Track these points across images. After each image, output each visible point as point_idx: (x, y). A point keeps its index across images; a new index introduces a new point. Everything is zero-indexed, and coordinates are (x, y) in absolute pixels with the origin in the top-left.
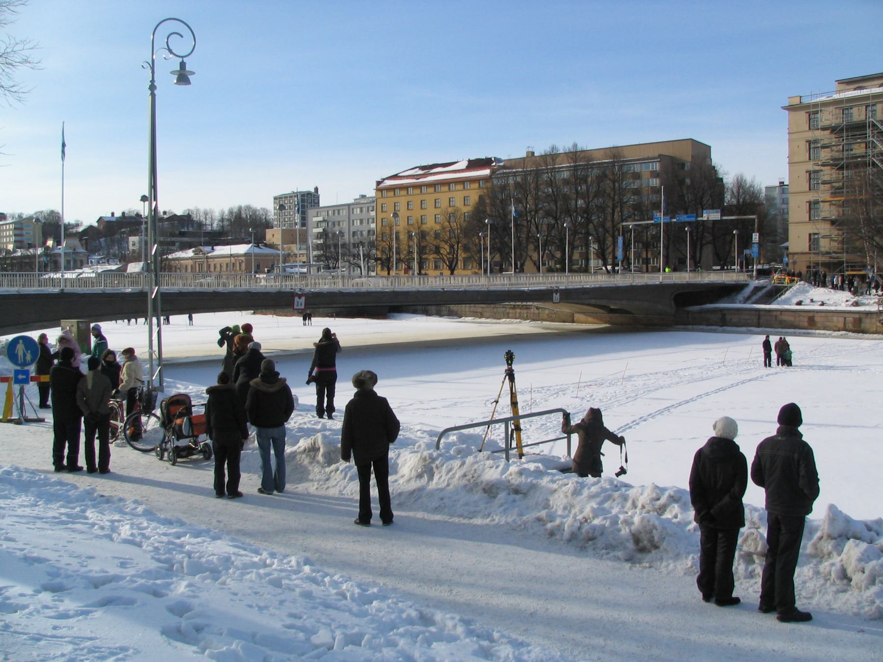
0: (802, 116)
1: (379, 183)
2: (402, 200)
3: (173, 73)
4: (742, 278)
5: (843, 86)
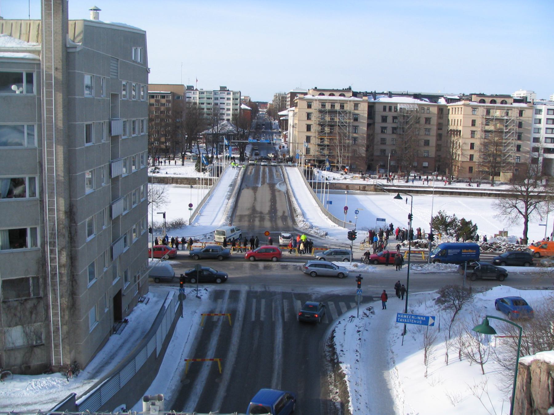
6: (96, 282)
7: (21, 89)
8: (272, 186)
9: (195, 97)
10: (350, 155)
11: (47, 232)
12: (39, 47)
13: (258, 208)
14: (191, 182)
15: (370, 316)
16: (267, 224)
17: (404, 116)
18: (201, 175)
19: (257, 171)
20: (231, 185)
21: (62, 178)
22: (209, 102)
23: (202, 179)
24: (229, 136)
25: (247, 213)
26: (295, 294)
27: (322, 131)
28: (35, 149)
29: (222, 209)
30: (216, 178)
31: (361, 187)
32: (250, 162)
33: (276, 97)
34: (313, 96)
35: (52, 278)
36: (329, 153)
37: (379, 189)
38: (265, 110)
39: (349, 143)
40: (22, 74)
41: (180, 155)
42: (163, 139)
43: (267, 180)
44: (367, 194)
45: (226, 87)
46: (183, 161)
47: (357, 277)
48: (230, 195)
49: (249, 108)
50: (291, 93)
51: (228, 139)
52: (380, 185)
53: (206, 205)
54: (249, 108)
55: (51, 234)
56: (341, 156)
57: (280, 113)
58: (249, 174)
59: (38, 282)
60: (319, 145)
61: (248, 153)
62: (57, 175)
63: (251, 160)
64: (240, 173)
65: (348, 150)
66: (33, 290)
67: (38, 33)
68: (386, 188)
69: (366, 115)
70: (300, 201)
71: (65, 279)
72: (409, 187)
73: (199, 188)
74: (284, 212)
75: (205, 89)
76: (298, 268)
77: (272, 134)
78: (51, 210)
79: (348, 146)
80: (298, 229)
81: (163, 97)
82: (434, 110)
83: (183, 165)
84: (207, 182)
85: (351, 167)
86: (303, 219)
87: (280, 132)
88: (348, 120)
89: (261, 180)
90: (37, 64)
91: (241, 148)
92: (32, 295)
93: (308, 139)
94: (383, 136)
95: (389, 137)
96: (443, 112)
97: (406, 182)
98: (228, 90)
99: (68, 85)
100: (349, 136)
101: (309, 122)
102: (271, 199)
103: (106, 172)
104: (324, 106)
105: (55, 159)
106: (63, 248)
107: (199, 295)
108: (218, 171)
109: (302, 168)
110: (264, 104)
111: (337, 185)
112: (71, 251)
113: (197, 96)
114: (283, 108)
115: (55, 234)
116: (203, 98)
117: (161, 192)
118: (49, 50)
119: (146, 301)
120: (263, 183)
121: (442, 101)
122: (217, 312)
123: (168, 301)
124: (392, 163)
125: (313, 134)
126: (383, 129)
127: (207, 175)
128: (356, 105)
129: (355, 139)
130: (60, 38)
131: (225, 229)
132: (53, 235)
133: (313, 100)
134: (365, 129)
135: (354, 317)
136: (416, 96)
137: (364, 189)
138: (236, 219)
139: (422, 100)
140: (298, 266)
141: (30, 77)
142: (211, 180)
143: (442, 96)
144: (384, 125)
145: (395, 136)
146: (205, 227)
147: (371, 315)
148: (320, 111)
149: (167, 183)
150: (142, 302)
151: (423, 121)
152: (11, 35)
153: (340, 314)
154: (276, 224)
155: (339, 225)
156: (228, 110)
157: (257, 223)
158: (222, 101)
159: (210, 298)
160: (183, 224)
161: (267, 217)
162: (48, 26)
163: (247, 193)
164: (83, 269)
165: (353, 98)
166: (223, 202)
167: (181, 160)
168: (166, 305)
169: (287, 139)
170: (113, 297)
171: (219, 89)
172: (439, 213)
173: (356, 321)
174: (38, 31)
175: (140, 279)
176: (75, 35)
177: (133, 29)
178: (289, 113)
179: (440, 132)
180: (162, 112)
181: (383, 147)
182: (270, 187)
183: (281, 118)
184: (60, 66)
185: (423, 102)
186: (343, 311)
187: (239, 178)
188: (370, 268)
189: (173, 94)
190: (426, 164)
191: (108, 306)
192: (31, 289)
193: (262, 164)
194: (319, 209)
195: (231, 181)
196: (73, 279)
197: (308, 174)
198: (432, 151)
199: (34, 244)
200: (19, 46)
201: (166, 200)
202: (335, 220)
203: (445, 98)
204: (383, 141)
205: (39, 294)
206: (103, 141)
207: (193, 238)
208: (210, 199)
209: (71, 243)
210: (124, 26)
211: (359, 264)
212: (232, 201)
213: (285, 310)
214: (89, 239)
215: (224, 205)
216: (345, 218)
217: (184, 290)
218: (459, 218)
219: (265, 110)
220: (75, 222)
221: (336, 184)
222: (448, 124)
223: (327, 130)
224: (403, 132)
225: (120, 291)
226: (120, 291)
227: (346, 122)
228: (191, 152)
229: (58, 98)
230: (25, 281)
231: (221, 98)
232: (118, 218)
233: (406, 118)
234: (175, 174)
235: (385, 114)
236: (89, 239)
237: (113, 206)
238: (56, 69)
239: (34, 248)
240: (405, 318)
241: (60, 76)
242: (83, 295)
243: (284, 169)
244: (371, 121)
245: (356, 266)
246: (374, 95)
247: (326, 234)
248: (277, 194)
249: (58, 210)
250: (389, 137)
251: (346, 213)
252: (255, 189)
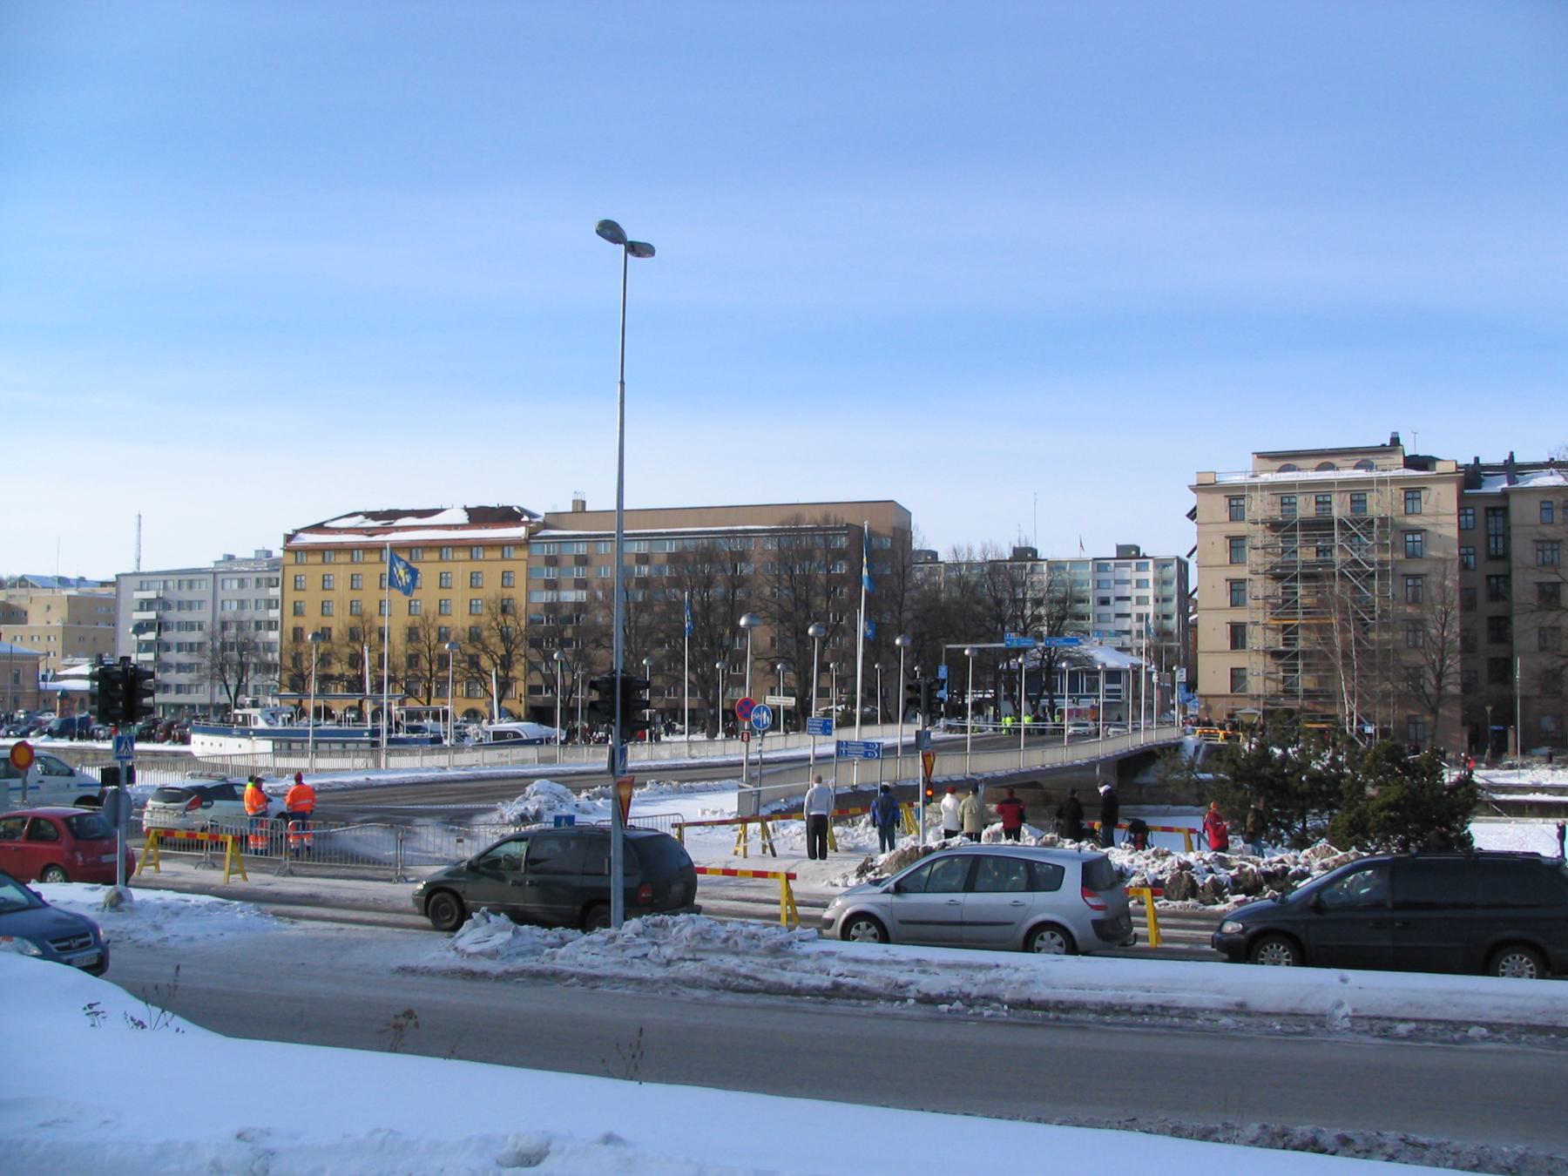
0: (1220, 503)
1: (289, 538)
2: (341, 572)
3: (1477, 459)
4: (1168, 735)
5: (1266, 463)
27: (1286, 606)
60: (1276, 655)
68: (1503, 797)
231: (1119, 599)
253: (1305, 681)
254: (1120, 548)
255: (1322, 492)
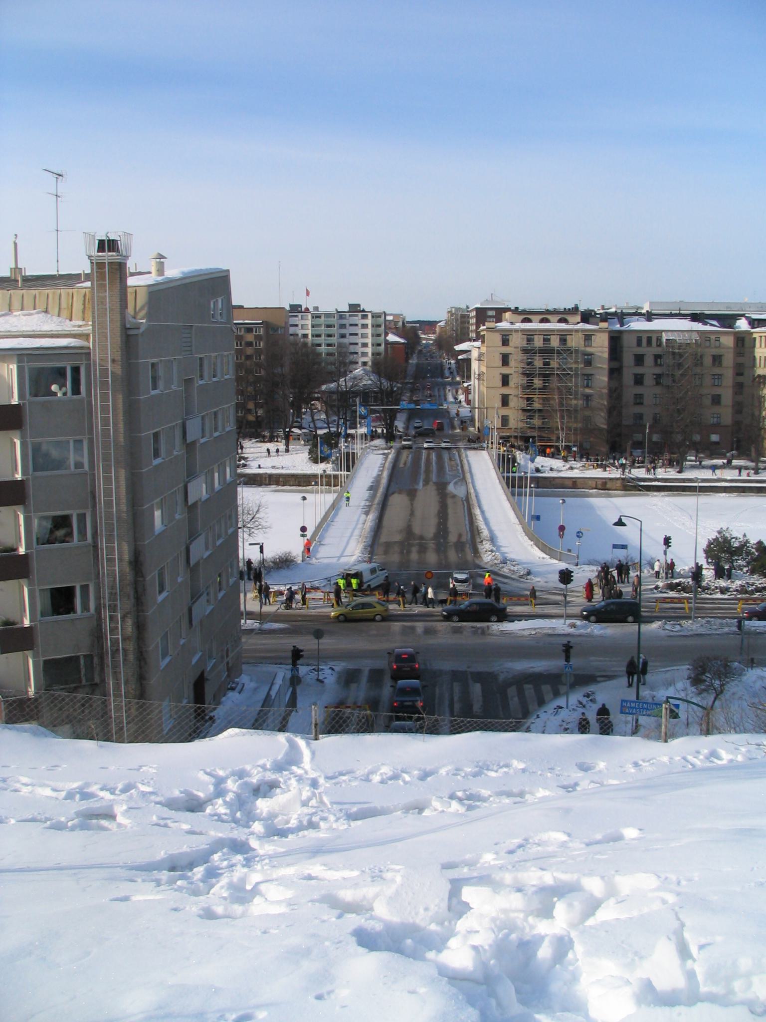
6: (170, 661)
7: (64, 389)
8: (441, 488)
9: (305, 327)
10: (580, 425)
11: (104, 591)
12: (88, 329)
13: (417, 530)
14: (301, 481)
15: (587, 706)
16: (432, 557)
17: (674, 353)
18: (318, 469)
19: (416, 460)
20: (371, 488)
21: (124, 515)
22: (329, 342)
23: (322, 476)
24: (366, 396)
25: (398, 538)
26: (472, 673)
27: (529, 386)
28: (86, 474)
29: (357, 532)
30: (346, 473)
31: (600, 482)
32: (404, 443)
33: (452, 315)
34: (512, 323)
35: (113, 657)
36: (543, 423)
37: (631, 487)
38: (433, 337)
39: (576, 405)
40: (64, 369)
41: (281, 434)
42: (251, 405)
43: (434, 477)
44: (610, 496)
45: (359, 305)
46: (287, 445)
47: (564, 645)
48: (370, 507)
49: (402, 341)
50: (478, 310)
51: (365, 403)
52: (633, 479)
53: (328, 526)
54: (402, 341)
55: (111, 594)
56: (562, 429)
57: (458, 348)
58: (401, 465)
59: (92, 662)
60: (524, 410)
61: (400, 424)
62: (118, 511)
63: (405, 440)
64: (387, 465)
65: (575, 418)
66: (85, 675)
67: (84, 308)
69: (606, 355)
70: (488, 515)
71: (131, 657)
72: (684, 480)
73: (317, 492)
74: (460, 536)
75: (322, 309)
76: (480, 631)
77: (444, 385)
78: (111, 561)
79: (576, 411)
80: (482, 564)
81: (249, 330)
82: (728, 341)
83: (287, 451)
84: (330, 481)
85: (581, 447)
86: (491, 547)
87: (459, 383)
88: (572, 364)
89: (422, 477)
90: (85, 353)
91: (389, 418)
92: (84, 682)
93: (505, 401)
94: (639, 390)
95: (649, 391)
96: (743, 342)
97: (679, 472)
98: (363, 311)
99: (129, 382)
100: (576, 393)
101: (505, 370)
102: (439, 512)
103: (180, 498)
104: (529, 340)
105: (112, 487)
106: (128, 613)
107: (321, 678)
108: (348, 460)
109: (494, 452)
110: (430, 325)
111: (558, 481)
112: (138, 616)
113: (309, 322)
114: (464, 337)
115: (116, 593)
116: (319, 325)
117: (256, 510)
118: (103, 335)
119: (239, 687)
120: (427, 482)
121: (742, 325)
122: (350, 702)
123: (276, 688)
124: (655, 438)
125: (512, 391)
126: (639, 380)
127: (327, 468)
128: (588, 337)
129: (587, 398)
130: (118, 317)
131: (364, 567)
132: (113, 595)
133: (511, 330)
134: (606, 379)
135: (561, 708)
136: (695, 317)
137: (604, 486)
138: (379, 550)
139: (705, 324)
140: (479, 628)
141: (76, 370)
142: (336, 477)
143: (743, 315)
144: (639, 370)
145: (658, 390)
146: (328, 566)
147: (590, 704)
148: (525, 351)
149: (260, 485)
150: (233, 689)
151: (708, 361)
152: (46, 312)
153: (541, 702)
154: (446, 557)
155: (552, 557)
156: (365, 345)
157: (414, 556)
158: (353, 330)
159: (338, 681)
160: (292, 561)
161: (431, 545)
162: (102, 302)
163: (398, 501)
164: (154, 642)
165: (582, 326)
166: (358, 520)
167: (284, 441)
168: (273, 693)
169: (470, 397)
170: (192, 682)
171: (347, 309)
172: (719, 532)
173: (563, 713)
174: (84, 304)
175: (231, 655)
176: (137, 304)
177: (212, 273)
178: (471, 348)
179: (740, 379)
180: (248, 357)
181: (638, 410)
182: (438, 489)
183: (460, 357)
184: (118, 357)
185: (708, 328)
186: (547, 698)
187: (385, 474)
188: (598, 629)
189: (266, 325)
190: (714, 438)
191: (186, 696)
192: (83, 672)
193: (425, 445)
194: (519, 528)
195: (371, 480)
196: (141, 657)
197: (505, 463)
198: (726, 415)
199: (85, 607)
200: (59, 328)
201: (264, 524)
202: (544, 548)
203: (747, 318)
204: (639, 400)
205: (93, 679)
206: (175, 453)
207: (308, 586)
208: (336, 515)
209: (138, 605)
210: (199, 274)
211: (578, 623)
212: (372, 517)
213: (456, 698)
214: (160, 598)
215: (360, 526)
216: (559, 546)
217: (298, 670)
218: (753, 541)
219: (433, 337)
220: (143, 576)
221: (554, 478)
222: (754, 366)
223: (538, 382)
224: (674, 381)
225: (202, 673)
226: (202, 673)
227: (571, 369)
228: (300, 428)
229: (115, 402)
230: (72, 661)
231: (351, 325)
232: (197, 564)
233: (677, 357)
234: (273, 467)
235: (640, 351)
236: (160, 598)
237: (191, 546)
238: (113, 361)
239: (86, 614)
240: (633, 708)
241: (119, 370)
242: (154, 680)
243: (464, 455)
244: (615, 365)
245: (573, 626)
246: (621, 316)
247: (529, 573)
248: (449, 501)
249: (120, 560)
250: (649, 391)
251: (561, 536)
252: (412, 494)
253: (537, 422)
254: (350, 306)
255: (546, 336)
